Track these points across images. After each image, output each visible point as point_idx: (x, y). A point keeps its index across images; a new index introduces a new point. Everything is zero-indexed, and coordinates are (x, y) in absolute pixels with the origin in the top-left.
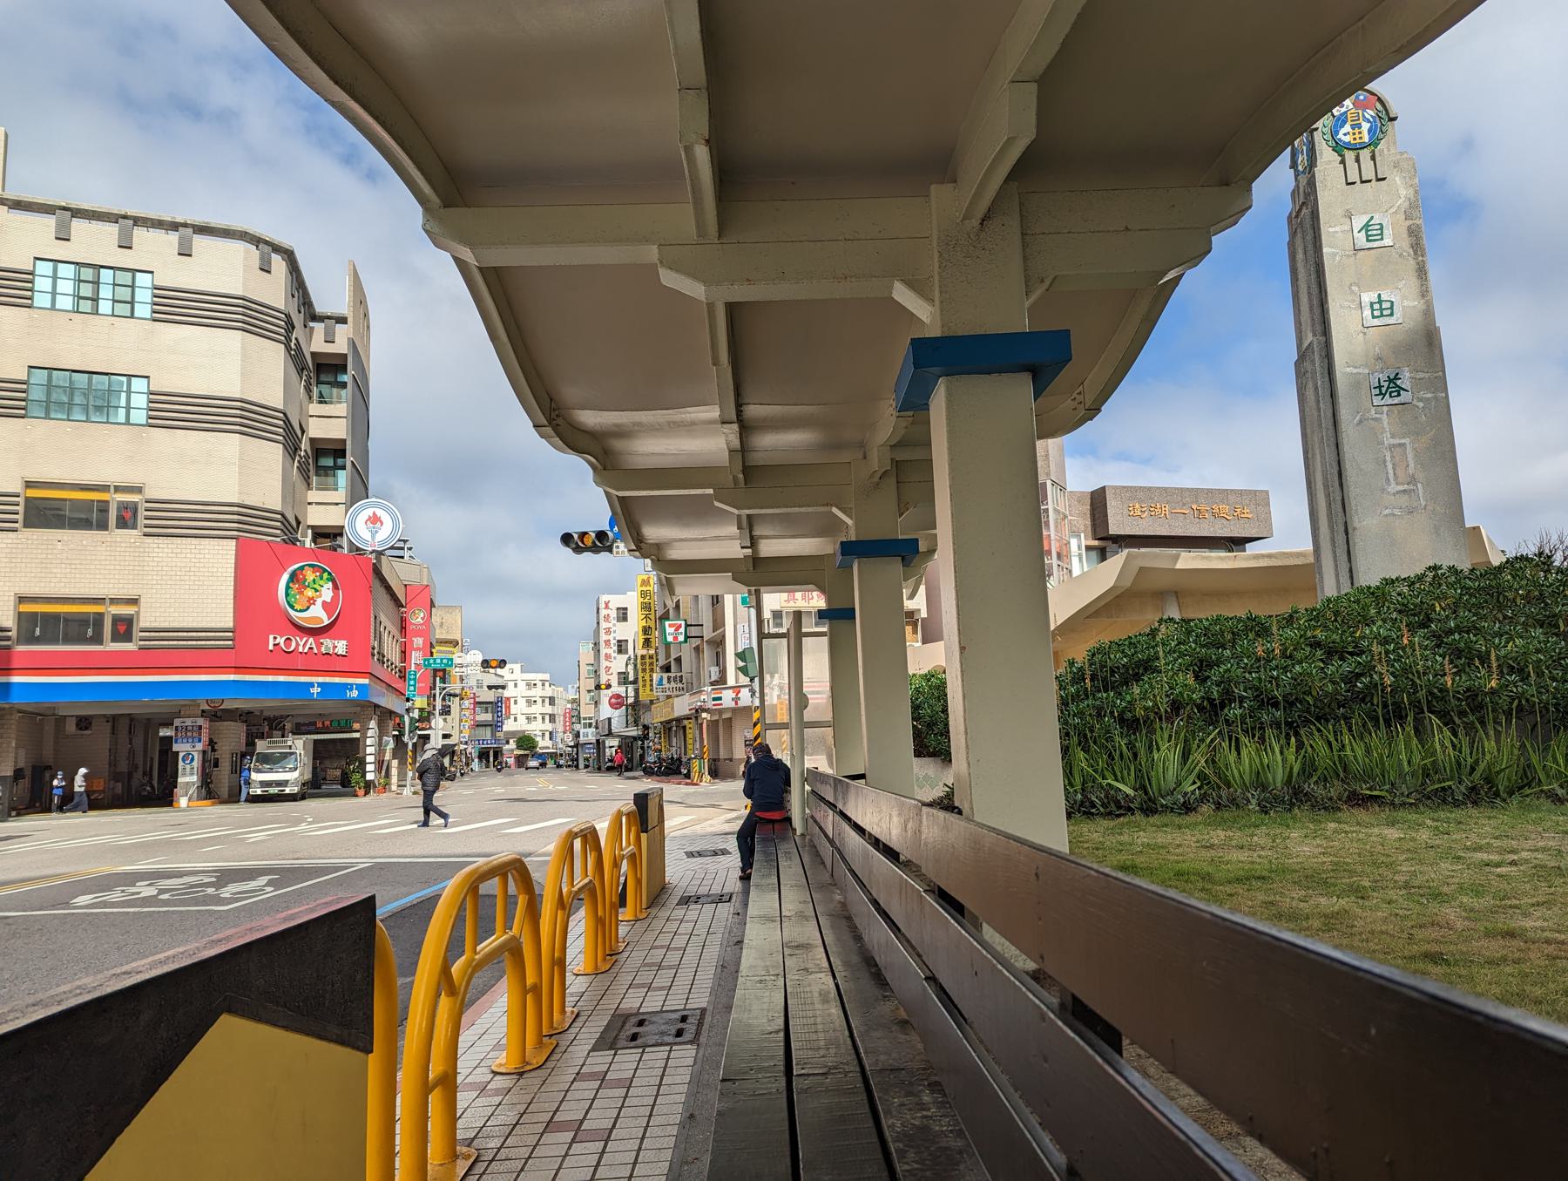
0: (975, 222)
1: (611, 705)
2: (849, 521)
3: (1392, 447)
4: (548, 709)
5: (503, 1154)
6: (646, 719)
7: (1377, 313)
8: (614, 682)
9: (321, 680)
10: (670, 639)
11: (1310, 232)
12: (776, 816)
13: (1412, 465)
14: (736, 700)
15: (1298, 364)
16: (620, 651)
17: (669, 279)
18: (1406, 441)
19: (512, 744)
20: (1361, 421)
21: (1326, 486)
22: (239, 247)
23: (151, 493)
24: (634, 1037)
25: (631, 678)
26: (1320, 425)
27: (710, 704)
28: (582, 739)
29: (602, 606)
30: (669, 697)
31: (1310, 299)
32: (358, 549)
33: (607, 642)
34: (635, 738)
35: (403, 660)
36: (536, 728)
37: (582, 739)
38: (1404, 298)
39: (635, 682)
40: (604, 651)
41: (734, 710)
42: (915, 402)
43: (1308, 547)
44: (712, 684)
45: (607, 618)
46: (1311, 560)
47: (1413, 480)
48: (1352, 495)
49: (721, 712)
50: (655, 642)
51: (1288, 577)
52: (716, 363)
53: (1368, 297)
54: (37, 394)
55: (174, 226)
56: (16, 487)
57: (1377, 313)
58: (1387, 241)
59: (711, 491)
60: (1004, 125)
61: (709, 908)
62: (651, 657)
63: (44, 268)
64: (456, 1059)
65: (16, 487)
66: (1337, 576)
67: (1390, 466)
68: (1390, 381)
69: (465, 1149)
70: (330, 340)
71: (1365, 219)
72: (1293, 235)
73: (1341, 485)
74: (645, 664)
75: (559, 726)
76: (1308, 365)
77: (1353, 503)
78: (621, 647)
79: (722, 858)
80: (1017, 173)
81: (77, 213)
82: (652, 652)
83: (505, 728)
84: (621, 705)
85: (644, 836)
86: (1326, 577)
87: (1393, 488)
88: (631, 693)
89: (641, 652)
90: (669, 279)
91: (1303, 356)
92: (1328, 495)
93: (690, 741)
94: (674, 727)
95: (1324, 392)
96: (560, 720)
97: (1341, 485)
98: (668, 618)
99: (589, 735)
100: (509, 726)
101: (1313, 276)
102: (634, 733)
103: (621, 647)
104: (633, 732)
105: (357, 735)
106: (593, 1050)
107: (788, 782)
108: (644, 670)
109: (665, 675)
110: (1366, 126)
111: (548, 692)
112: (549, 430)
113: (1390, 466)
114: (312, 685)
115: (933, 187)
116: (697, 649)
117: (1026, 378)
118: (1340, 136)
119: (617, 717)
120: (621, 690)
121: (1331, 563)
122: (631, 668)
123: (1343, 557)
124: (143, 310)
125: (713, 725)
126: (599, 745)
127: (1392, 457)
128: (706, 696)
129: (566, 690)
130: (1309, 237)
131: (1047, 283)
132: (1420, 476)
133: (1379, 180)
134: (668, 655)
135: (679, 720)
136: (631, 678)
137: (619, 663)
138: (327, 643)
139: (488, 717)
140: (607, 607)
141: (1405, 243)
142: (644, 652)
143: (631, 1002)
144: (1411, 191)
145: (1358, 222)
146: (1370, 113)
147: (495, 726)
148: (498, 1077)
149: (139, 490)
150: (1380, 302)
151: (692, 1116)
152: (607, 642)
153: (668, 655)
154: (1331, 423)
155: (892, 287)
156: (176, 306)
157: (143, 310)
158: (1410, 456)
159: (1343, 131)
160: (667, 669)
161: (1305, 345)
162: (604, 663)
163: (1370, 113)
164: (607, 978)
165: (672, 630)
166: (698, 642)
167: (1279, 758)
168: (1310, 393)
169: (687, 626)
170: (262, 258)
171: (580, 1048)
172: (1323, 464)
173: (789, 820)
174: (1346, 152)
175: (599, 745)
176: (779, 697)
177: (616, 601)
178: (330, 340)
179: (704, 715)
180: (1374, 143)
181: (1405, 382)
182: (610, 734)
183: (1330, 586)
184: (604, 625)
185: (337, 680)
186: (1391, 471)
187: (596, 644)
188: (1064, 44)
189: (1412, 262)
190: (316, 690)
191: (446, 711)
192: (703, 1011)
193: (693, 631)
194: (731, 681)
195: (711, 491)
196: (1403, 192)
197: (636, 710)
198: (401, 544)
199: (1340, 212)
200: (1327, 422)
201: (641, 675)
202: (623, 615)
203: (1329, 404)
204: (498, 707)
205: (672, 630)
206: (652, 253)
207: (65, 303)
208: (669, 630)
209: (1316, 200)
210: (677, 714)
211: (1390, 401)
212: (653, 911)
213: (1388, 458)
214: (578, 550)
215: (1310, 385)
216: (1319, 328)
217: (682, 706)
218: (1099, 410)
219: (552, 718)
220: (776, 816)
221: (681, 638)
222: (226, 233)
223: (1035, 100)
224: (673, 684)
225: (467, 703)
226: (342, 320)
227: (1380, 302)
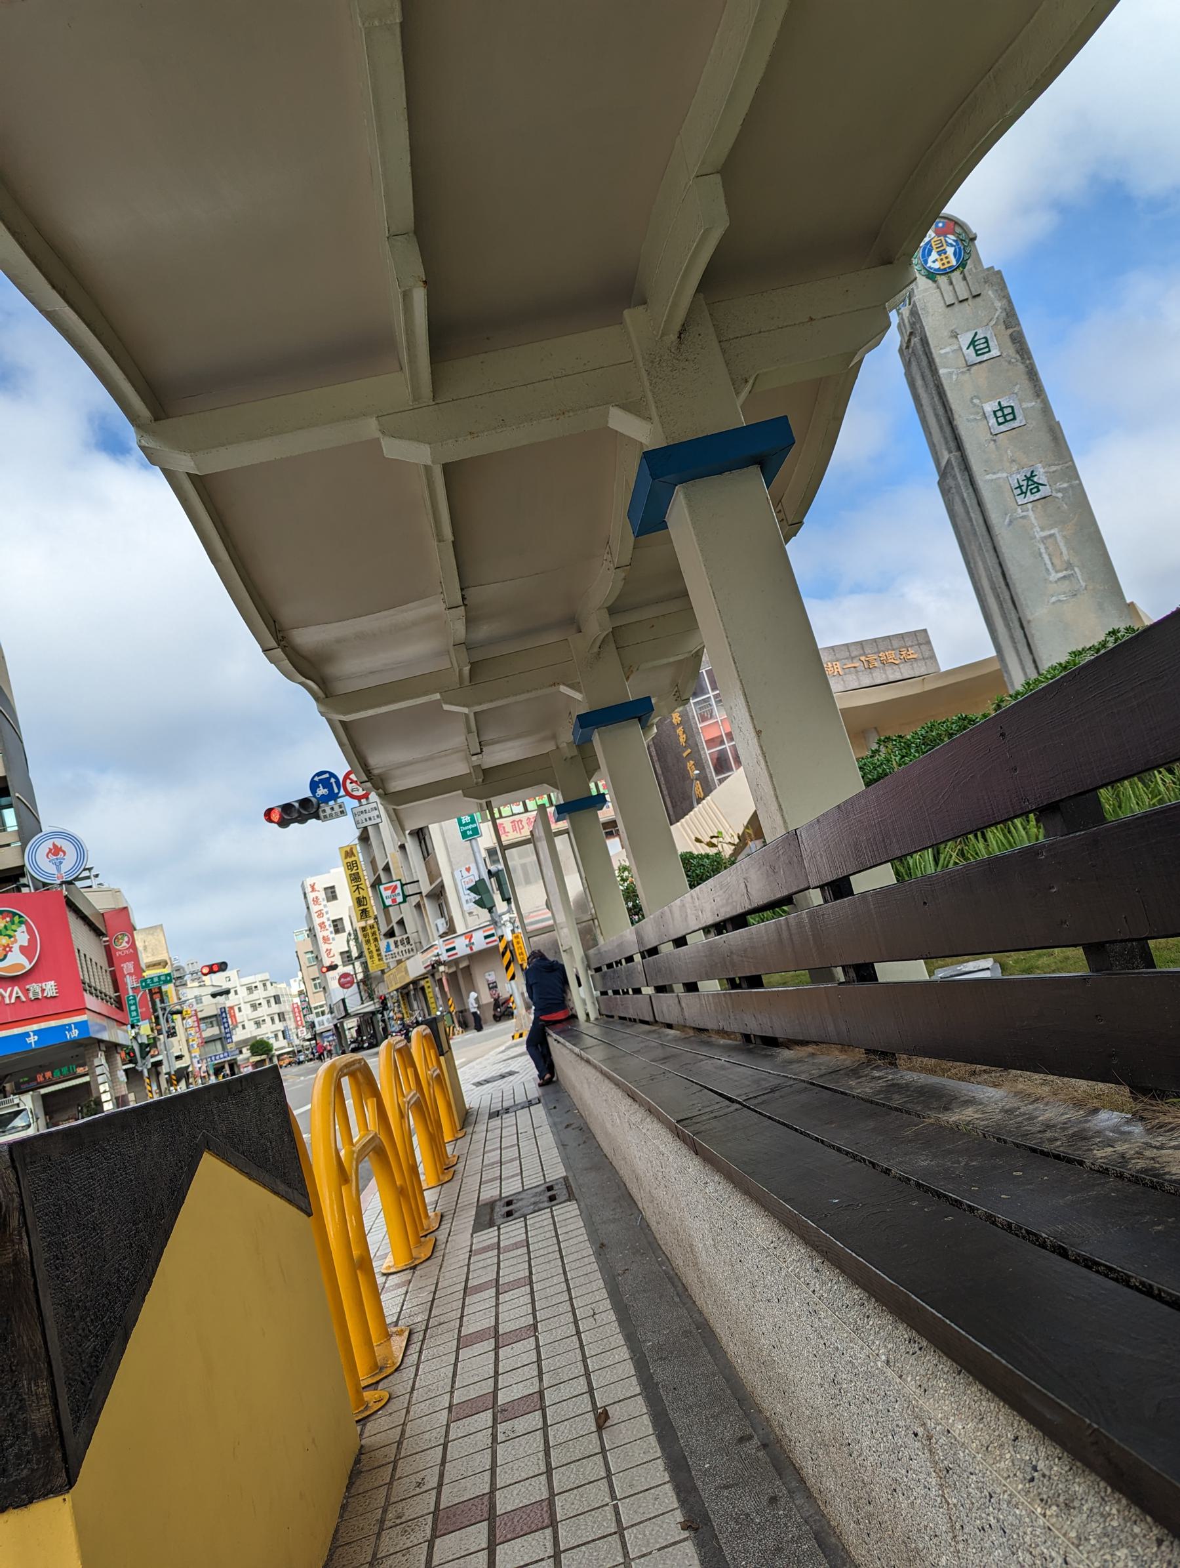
0: (673, 337)
1: (342, 985)
2: (577, 696)
3: (1044, 540)
4: (275, 1008)
5: (432, 1322)
6: (381, 990)
7: (1001, 420)
8: (338, 960)
9: (35, 1027)
10: (388, 902)
11: (924, 358)
12: (560, 1015)
13: (1065, 551)
14: (470, 945)
15: (940, 484)
16: (337, 931)
17: (393, 449)
19: (246, 1052)
20: (1011, 522)
21: (994, 589)
24: (509, 1214)
25: (355, 954)
26: (975, 533)
27: (444, 957)
28: (318, 1029)
29: (309, 889)
30: (399, 962)
31: (939, 421)
32: (45, 885)
33: (322, 925)
34: (373, 1013)
35: (116, 990)
36: (266, 1032)
37: (318, 1029)
38: (1021, 401)
39: (361, 956)
40: (320, 934)
41: (470, 957)
42: (650, 519)
43: (993, 653)
44: (441, 937)
45: (316, 900)
46: (997, 666)
47: (1069, 566)
48: (1019, 590)
49: (456, 962)
50: (374, 908)
51: (976, 681)
52: (440, 539)
53: (990, 407)
57: (1001, 420)
58: (995, 352)
59: (438, 696)
60: (688, 230)
61: (523, 1115)
62: (372, 927)
64: (365, 1236)
66: (1023, 669)
67: (1046, 557)
68: (1028, 479)
69: (394, 1329)
71: (970, 336)
72: (907, 365)
73: (1007, 585)
74: (367, 935)
75: (291, 1024)
76: (950, 482)
77: (1022, 598)
78: (337, 926)
79: (511, 1078)
80: (703, 286)
82: (371, 921)
83: (235, 1038)
84: (352, 983)
85: (442, 1058)
86: (1013, 673)
87: (1054, 576)
88: (359, 968)
89: (359, 925)
90: (393, 449)
91: (944, 474)
92: (997, 597)
93: (431, 1000)
94: (411, 991)
95: (971, 502)
96: (289, 1016)
97: (1007, 585)
98: (381, 884)
99: (325, 1023)
100: (239, 1035)
101: (936, 399)
102: (372, 1009)
103: (337, 926)
104: (370, 1007)
105: (87, 1079)
106: (474, 1232)
107: (565, 982)
108: (368, 942)
109: (391, 941)
110: (950, 251)
111: (271, 991)
112: (279, 652)
113: (1046, 557)
114: (27, 1035)
115: (626, 312)
116: (418, 906)
117: (755, 470)
118: (930, 264)
119: (352, 996)
120: (349, 969)
121: (1015, 658)
122: (352, 943)
123: (1024, 650)
125: (452, 977)
126: (338, 1030)
127: (1046, 548)
128: (440, 949)
129: (289, 985)
130: (924, 363)
131: (751, 382)
133: (975, 297)
134: (388, 920)
135: (415, 982)
136: (355, 954)
137: (340, 943)
138: (35, 988)
139: (214, 1031)
140: (313, 889)
141: (1011, 351)
142: (363, 924)
143: (490, 1192)
145: (965, 339)
146: (951, 238)
147: (223, 1039)
148: (391, 1277)
150: (1001, 409)
151: (602, 1245)
152: (322, 925)
153: (388, 920)
154: (984, 529)
155: (606, 416)
158: (1062, 544)
159: (931, 259)
160: (391, 934)
161: (943, 463)
162: (323, 947)
163: (951, 238)
164: (455, 1185)
165: (389, 893)
166: (416, 899)
167: (1023, 833)
168: (958, 507)
169: (402, 885)
171: (460, 1235)
172: (987, 569)
173: (574, 1017)
174: (938, 277)
175: (338, 1030)
176: (513, 931)
177: (322, 882)
179: (442, 968)
180: (962, 265)
181: (1041, 477)
182: (347, 1015)
183: (1018, 680)
184: (314, 909)
185: (53, 1023)
187: (311, 929)
189: (1021, 366)
190: (32, 1039)
191: (172, 1033)
192: (565, 1179)
194: (460, 928)
195: (438, 696)
197: (368, 984)
198: (86, 874)
199: (946, 333)
200: (981, 529)
201: (365, 947)
202: (331, 893)
203: (978, 512)
204: (222, 1018)
205: (389, 893)
206: (371, 427)
208: (386, 894)
209: (922, 327)
210: (413, 975)
211: (1033, 498)
212: (469, 1130)
213: (1043, 550)
214: (283, 823)
215: (957, 499)
216: (952, 445)
217: (416, 966)
218: (801, 523)
219: (282, 1017)
220: (560, 1015)
221: (400, 899)
223: (721, 190)
224: (401, 948)
225: (190, 1022)
227: (1001, 409)
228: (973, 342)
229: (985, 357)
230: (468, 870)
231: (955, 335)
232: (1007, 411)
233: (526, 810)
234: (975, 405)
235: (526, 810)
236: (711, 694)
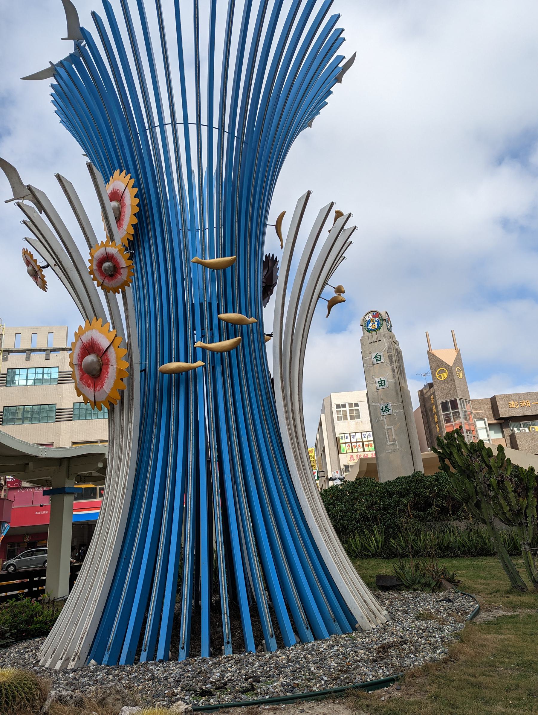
13: (394, 435)
20: (378, 421)
53: (377, 380)
54: (76, 412)
58: (382, 361)
67: (387, 436)
68: (386, 407)
87: (389, 443)
110: (376, 323)
113: (387, 436)
118: (369, 327)
132: (396, 439)
144: (389, 343)
145: (373, 355)
150: (381, 381)
158: (393, 432)
159: (369, 325)
169: (318, 472)
188: (60, 561)
189: (390, 367)
193: (321, 474)
196: (386, 344)
228: (376, 356)
229: (379, 362)
230: (337, 472)
231: (371, 353)
232: (383, 382)
233: (364, 451)
234: (373, 378)
235: (364, 451)
236: (451, 411)
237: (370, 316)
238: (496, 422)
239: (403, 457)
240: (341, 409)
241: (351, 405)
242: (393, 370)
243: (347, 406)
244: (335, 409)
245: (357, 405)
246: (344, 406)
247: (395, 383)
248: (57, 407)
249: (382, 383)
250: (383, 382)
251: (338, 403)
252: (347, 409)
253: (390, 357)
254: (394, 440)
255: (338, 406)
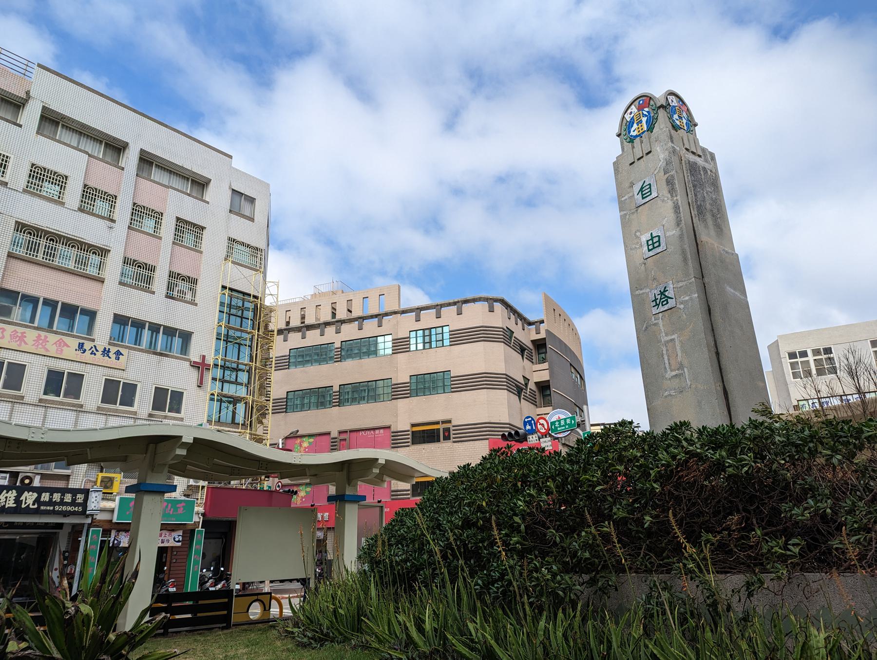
18: (674, 336)
20: (647, 328)
22: (478, 304)
23: (454, 423)
53: (645, 238)
55: (455, 303)
56: (407, 427)
63: (413, 334)
65: (408, 427)
67: (666, 357)
70: (538, 333)
71: (641, 184)
81: (466, 301)
87: (670, 374)
110: (644, 119)
113: (666, 357)
124: (447, 342)
127: (667, 350)
132: (685, 362)
144: (667, 153)
145: (637, 188)
149: (449, 422)
150: (652, 239)
156: (460, 337)
157: (447, 342)
158: (678, 348)
159: (633, 129)
170: (489, 307)
178: (538, 333)
186: (667, 362)
207: (420, 346)
222: (474, 300)
226: (542, 322)
231: (632, 185)
232: (655, 240)
237: (634, 109)
238: (148, 455)
239: (699, 402)
240: (799, 360)
241: (816, 352)
242: (676, 208)
243: (810, 353)
244: (787, 362)
245: (828, 351)
246: (804, 354)
247: (681, 237)
248: (394, 382)
249: (654, 243)
250: (655, 240)
251: (791, 350)
252: (811, 358)
253: (670, 182)
254: (681, 367)
255: (792, 355)
